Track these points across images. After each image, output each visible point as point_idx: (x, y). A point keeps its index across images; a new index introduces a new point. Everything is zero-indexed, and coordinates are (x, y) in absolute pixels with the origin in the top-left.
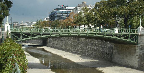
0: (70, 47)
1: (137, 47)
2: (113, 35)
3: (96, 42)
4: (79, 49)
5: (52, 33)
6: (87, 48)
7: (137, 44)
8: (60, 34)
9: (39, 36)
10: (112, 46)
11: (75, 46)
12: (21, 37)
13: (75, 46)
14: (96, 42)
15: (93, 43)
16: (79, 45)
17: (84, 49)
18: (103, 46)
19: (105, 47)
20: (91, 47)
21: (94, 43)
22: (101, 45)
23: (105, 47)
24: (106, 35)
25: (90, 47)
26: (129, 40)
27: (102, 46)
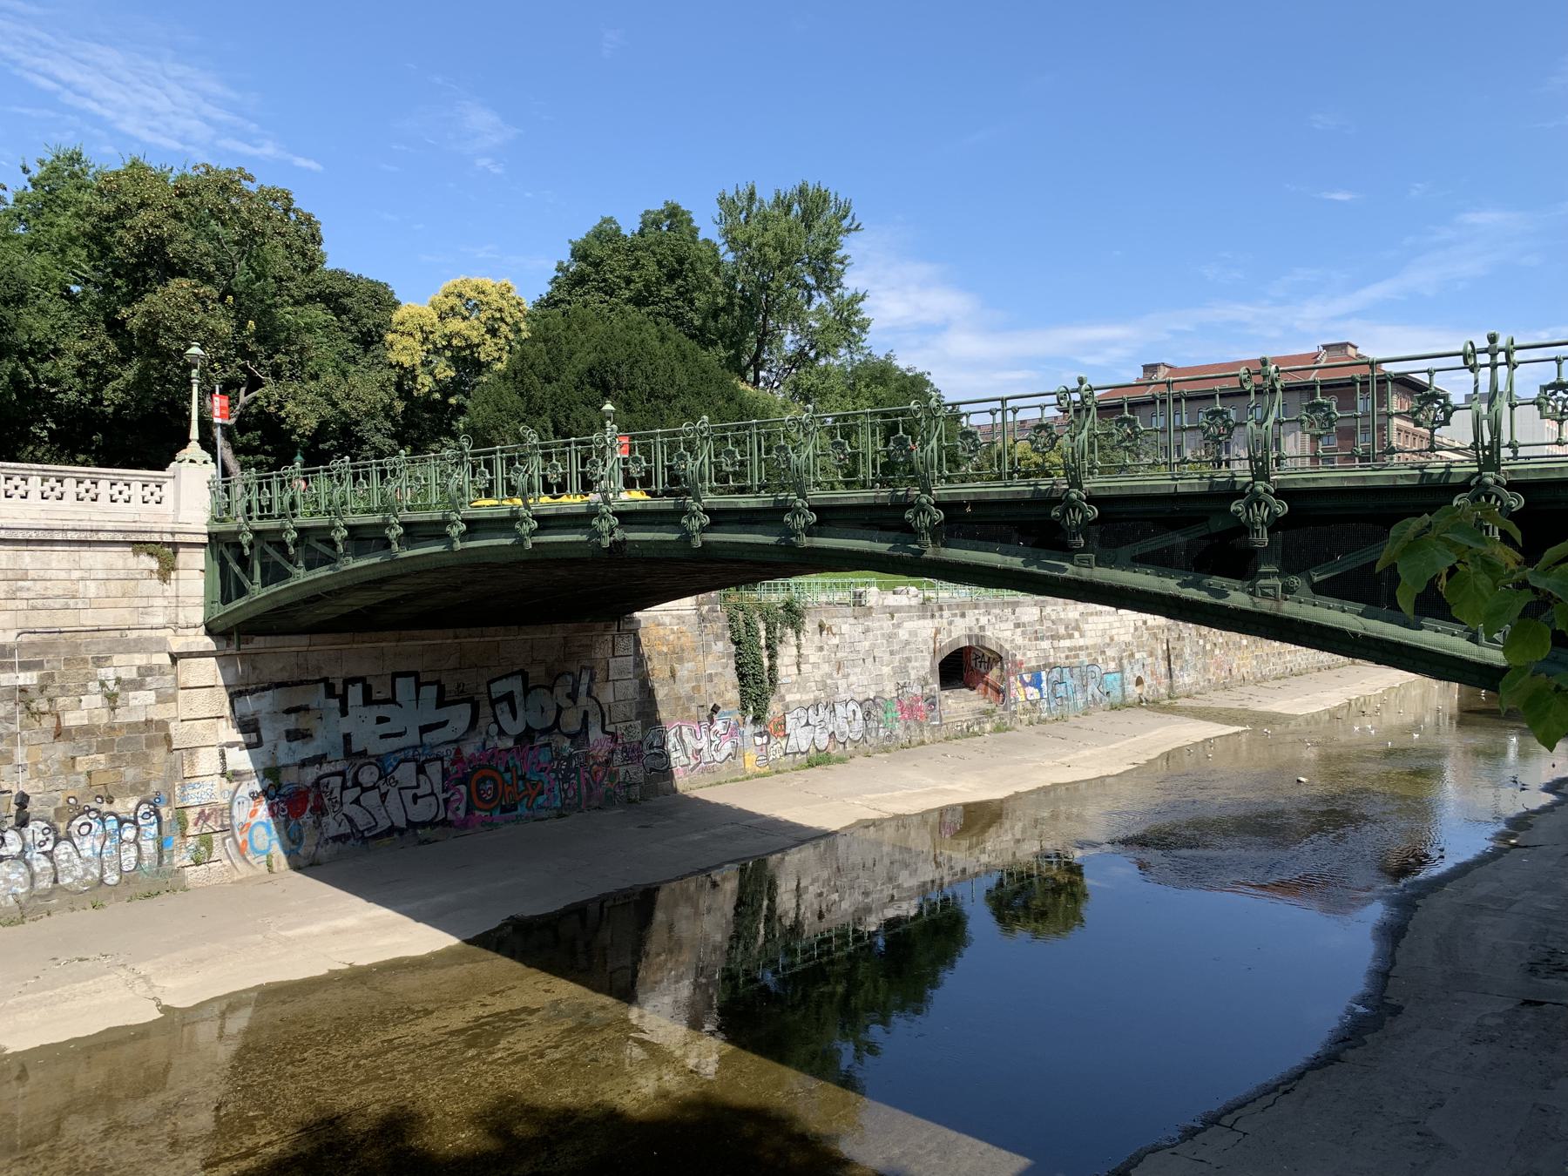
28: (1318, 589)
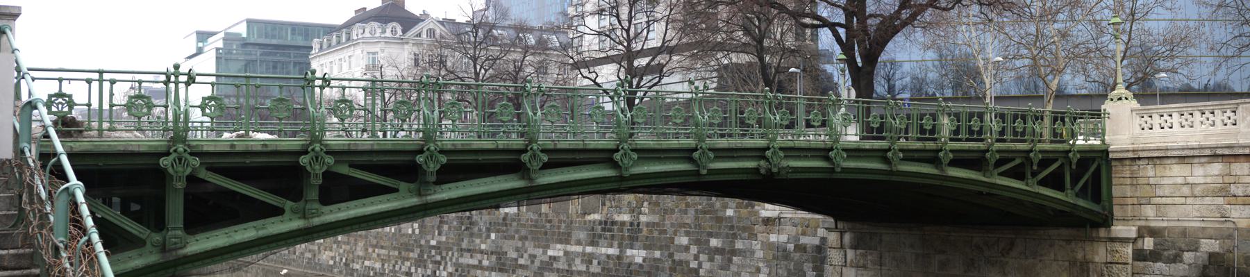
0: (383, 252)
1: (1113, 240)
2: (433, 167)
3: (643, 219)
4: (474, 267)
5: (545, 158)
6: (554, 258)
7: (1106, 221)
8: (615, 165)
9: (403, 186)
10: (809, 241)
11: (433, 243)
12: (175, 209)
13: (433, 247)
14: (643, 219)
15: (608, 225)
16: (472, 235)
17: (521, 261)
18: (714, 242)
19: (739, 245)
20: (589, 249)
21: (614, 223)
22: (687, 234)
23: (734, 252)
24: (955, 163)
25: (584, 254)
26: (1067, 197)
27: (701, 243)
28: (1001, 174)
